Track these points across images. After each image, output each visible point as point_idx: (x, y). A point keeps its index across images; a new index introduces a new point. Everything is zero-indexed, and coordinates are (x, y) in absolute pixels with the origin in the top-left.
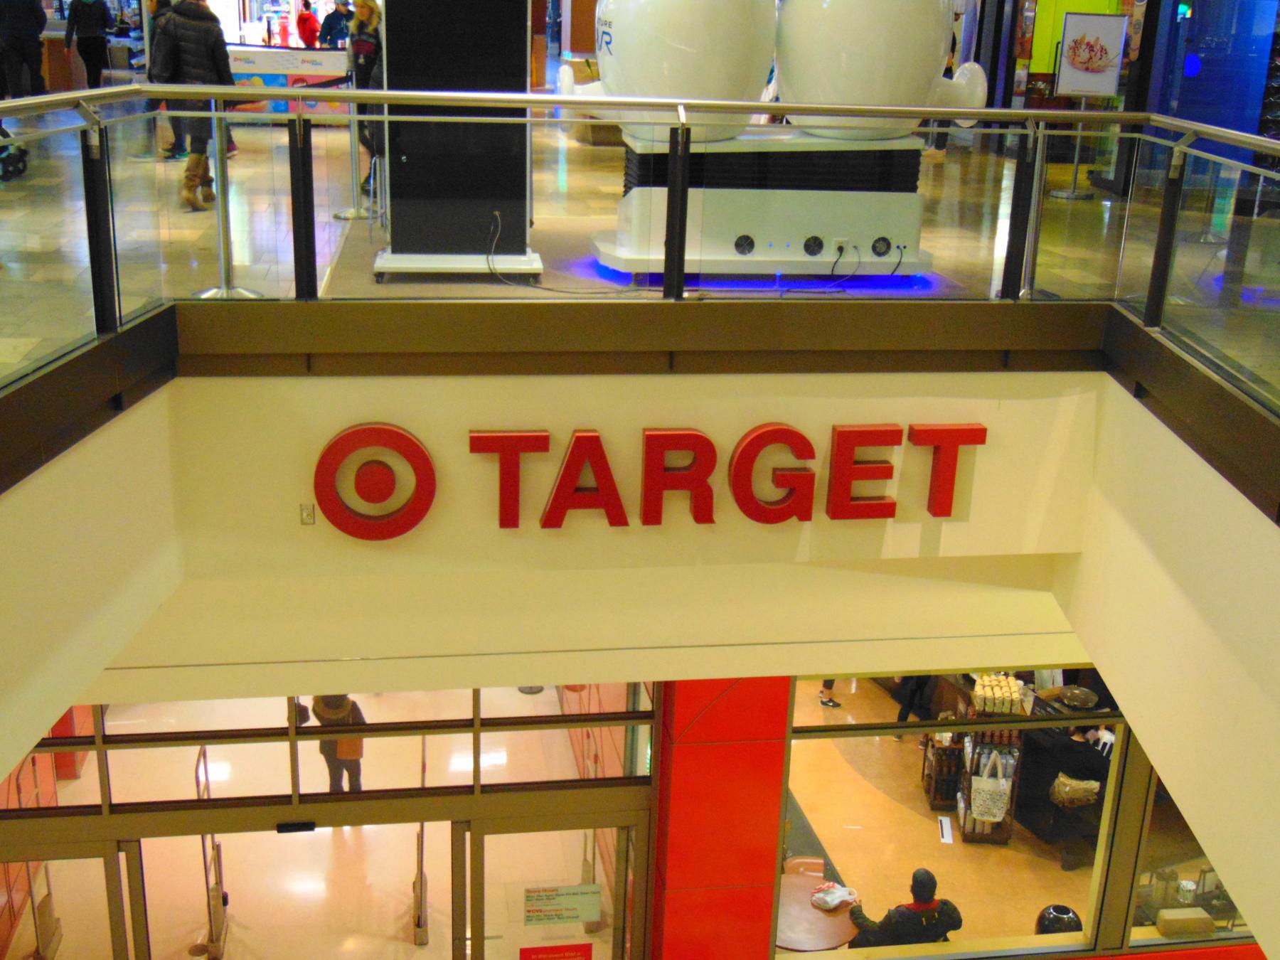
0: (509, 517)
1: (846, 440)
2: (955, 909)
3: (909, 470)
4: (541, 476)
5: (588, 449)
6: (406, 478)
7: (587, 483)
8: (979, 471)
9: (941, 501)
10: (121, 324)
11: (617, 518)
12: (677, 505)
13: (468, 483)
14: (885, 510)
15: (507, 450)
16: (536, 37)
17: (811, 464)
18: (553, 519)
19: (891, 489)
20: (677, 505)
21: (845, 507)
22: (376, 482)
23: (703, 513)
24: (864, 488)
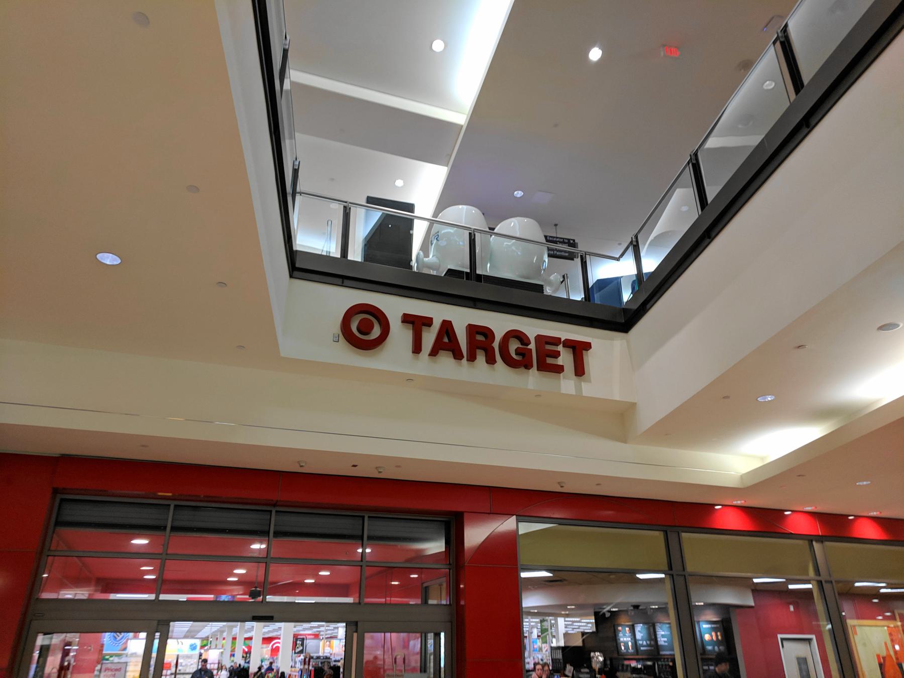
0: (417, 348)
1: (541, 340)
2: (598, 280)
3: (565, 358)
4: (429, 338)
5: (447, 328)
6: (376, 332)
7: (446, 341)
8: (591, 359)
9: (580, 370)
10: (49, 550)
11: (458, 355)
12: (481, 358)
13: (400, 335)
14: (559, 369)
15: (417, 323)
16: (266, 528)
17: (529, 347)
18: (434, 353)
19: (560, 361)
20: (481, 358)
21: (543, 367)
22: (365, 328)
23: (491, 360)
24: (550, 361)
